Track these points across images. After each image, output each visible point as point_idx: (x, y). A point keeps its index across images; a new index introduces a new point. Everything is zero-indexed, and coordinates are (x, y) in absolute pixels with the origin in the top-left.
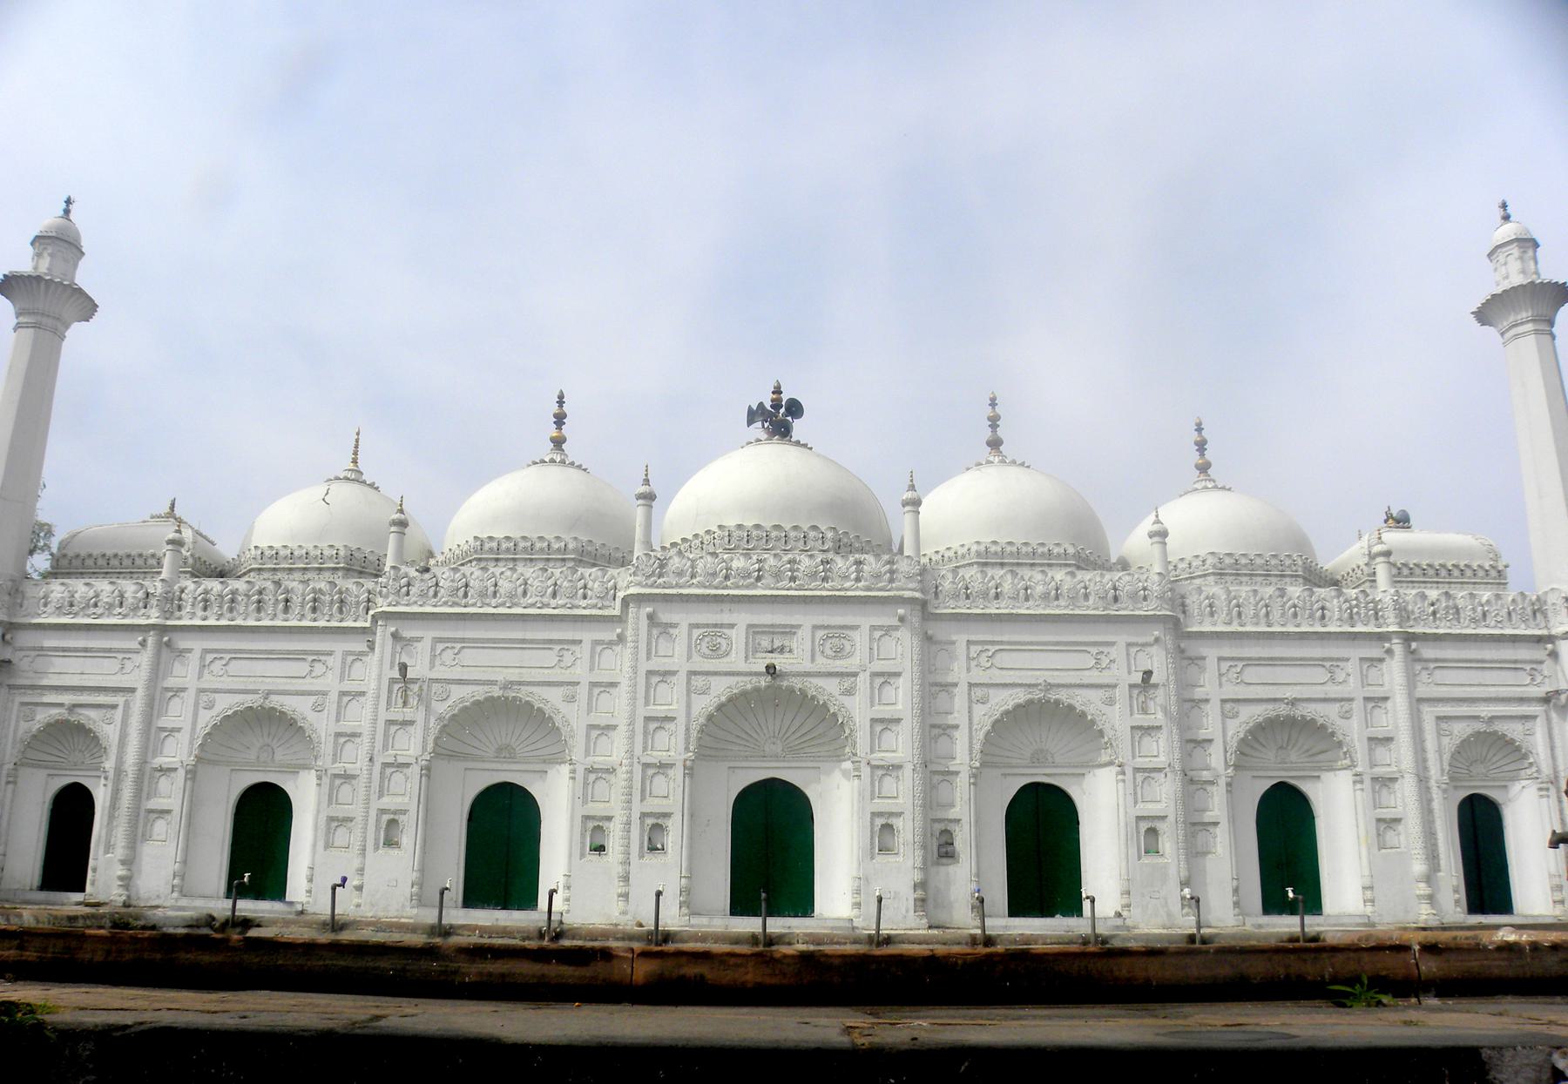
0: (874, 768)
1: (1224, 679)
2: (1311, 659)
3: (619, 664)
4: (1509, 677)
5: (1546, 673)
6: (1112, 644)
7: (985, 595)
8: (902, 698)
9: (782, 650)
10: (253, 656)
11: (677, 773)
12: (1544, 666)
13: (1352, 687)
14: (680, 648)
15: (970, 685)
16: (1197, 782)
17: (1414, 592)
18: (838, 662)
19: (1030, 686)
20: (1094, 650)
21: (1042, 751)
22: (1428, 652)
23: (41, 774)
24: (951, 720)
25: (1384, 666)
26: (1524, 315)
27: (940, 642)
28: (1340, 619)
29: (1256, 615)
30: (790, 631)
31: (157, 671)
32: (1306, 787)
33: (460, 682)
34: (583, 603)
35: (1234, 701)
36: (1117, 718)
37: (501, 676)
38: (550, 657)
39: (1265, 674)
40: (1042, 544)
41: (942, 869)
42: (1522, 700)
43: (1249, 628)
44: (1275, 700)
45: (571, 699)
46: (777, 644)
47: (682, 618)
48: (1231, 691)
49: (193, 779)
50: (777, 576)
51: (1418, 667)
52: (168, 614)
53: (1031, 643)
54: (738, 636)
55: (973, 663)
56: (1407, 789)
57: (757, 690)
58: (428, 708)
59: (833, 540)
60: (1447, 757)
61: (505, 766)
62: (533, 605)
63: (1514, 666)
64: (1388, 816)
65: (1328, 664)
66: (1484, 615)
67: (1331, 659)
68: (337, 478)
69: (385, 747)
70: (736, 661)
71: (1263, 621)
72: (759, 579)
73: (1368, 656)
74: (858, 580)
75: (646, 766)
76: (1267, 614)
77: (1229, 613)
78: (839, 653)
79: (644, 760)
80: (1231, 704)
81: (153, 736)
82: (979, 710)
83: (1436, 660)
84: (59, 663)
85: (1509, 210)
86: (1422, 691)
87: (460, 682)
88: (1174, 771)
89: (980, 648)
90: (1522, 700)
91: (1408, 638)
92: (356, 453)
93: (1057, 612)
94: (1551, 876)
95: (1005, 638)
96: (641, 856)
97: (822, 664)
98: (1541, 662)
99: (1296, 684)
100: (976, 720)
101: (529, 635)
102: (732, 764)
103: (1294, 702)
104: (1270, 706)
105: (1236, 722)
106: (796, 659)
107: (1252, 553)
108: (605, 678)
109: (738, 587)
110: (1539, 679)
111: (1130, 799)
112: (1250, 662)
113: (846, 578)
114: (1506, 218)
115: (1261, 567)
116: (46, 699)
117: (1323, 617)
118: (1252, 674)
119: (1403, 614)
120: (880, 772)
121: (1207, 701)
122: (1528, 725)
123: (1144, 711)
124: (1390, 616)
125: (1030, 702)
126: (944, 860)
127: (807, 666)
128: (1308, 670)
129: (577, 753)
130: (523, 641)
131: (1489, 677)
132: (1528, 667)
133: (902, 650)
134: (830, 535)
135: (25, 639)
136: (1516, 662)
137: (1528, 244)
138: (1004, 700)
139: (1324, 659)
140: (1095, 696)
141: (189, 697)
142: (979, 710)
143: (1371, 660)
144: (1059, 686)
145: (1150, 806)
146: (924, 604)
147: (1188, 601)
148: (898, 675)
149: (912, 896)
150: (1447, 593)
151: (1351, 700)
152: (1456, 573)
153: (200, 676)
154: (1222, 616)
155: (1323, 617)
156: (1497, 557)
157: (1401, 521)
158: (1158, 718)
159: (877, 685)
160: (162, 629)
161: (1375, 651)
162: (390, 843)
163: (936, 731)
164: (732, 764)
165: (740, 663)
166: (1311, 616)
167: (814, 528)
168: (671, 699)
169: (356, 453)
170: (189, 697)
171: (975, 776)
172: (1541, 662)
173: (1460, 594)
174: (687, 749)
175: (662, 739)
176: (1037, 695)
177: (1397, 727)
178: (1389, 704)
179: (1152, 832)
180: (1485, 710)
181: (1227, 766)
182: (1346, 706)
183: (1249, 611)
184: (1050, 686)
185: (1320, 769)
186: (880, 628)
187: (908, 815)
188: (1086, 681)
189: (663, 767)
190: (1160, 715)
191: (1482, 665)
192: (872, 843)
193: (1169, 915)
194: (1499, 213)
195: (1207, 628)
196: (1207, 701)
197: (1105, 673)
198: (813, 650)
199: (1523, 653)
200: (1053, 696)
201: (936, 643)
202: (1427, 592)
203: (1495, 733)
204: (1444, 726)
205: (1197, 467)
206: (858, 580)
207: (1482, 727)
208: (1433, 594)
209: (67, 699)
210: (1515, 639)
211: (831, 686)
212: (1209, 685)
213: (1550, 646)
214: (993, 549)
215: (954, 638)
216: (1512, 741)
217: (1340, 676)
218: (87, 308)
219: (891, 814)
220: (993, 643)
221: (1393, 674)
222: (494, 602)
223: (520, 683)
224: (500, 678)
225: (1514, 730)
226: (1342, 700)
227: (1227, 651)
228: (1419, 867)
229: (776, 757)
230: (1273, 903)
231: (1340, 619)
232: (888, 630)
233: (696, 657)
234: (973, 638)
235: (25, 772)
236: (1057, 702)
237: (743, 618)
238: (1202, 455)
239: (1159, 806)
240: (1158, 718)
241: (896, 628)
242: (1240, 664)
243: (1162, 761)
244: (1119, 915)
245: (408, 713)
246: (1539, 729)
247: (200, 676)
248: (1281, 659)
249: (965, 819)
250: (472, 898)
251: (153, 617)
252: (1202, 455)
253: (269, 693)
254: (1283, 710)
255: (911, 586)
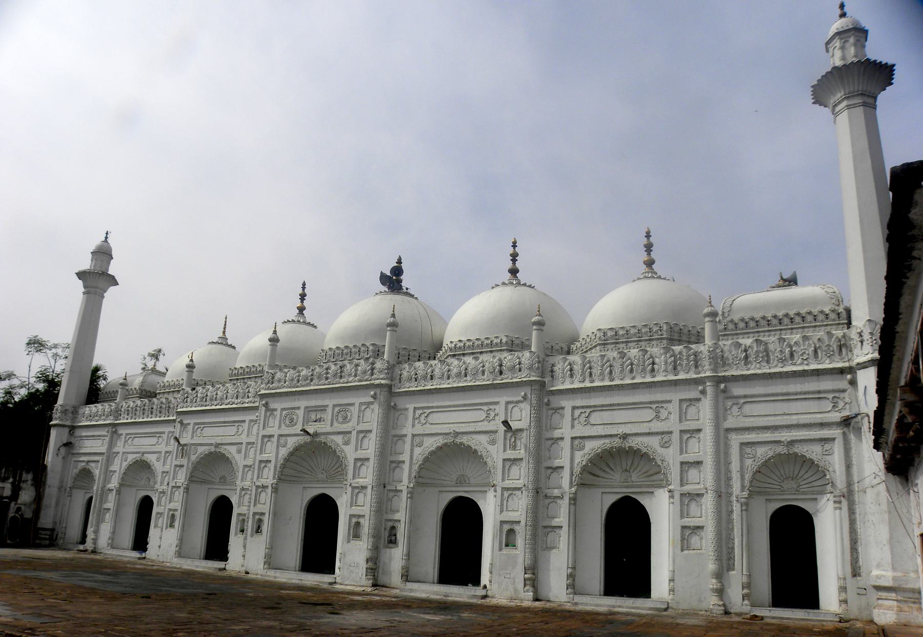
0: (354, 488)
1: (576, 422)
2: (641, 403)
4: (813, 406)
5: (847, 400)
6: (497, 403)
7: (425, 378)
9: (319, 420)
12: (846, 395)
13: (673, 424)
15: (414, 436)
16: (550, 497)
17: (730, 342)
18: (344, 426)
19: (446, 434)
20: (485, 408)
21: (463, 475)
22: (738, 390)
23: (82, 492)
24: (401, 458)
25: (700, 404)
26: (839, 95)
27: (400, 410)
28: (665, 371)
29: (602, 374)
31: (111, 445)
32: (645, 501)
33: (201, 445)
34: (247, 400)
35: (581, 438)
39: (606, 416)
40: (487, 338)
41: (388, 550)
42: (822, 425)
43: (597, 384)
44: (611, 436)
45: (493, 442)
46: (318, 417)
47: (276, 405)
48: (580, 431)
49: (575, 504)
50: (319, 377)
51: (729, 403)
53: (450, 406)
55: (417, 421)
57: (306, 443)
58: (189, 459)
59: (373, 352)
60: (748, 477)
61: (222, 487)
62: (228, 404)
63: (818, 396)
64: (692, 524)
65: (654, 406)
66: (792, 355)
67: (657, 402)
68: (639, 279)
69: (173, 479)
71: (607, 378)
72: (312, 380)
73: (836, 388)
74: (355, 376)
75: (258, 487)
76: (611, 372)
77: (583, 373)
78: (345, 420)
79: (258, 484)
80: (578, 441)
81: (108, 473)
82: (417, 451)
83: (745, 396)
84: (88, 443)
85: (846, 9)
86: (730, 423)
87: (201, 445)
88: (528, 490)
89: (421, 411)
90: (822, 425)
91: (718, 380)
92: (225, 328)
93: (465, 384)
94: (839, 578)
95: (435, 405)
96: (252, 536)
97: (338, 427)
98: (844, 391)
100: (415, 458)
101: (227, 419)
102: (441, 489)
103: (625, 437)
104: (607, 441)
105: (582, 453)
107: (627, 325)
108: (692, 425)
109: (303, 386)
110: (841, 404)
111: (498, 509)
112: (595, 408)
113: (350, 375)
114: (843, 15)
115: (635, 334)
116: (81, 459)
117: (653, 370)
120: (357, 491)
121: (562, 439)
122: (827, 446)
123: (514, 447)
124: (706, 363)
125: (446, 444)
126: (391, 545)
127: (328, 429)
128: (639, 412)
129: (498, 479)
130: (224, 422)
131: (795, 407)
132: (830, 396)
134: (371, 348)
135: (78, 432)
136: (819, 392)
137: (860, 33)
138: (431, 444)
139: (651, 403)
140: (483, 438)
142: (417, 451)
143: (690, 400)
144: (463, 433)
145: (510, 514)
146: (390, 387)
147: (555, 368)
148: (370, 431)
149: (365, 566)
150: (757, 340)
151: (671, 432)
152: (786, 321)
153: (573, 427)
154: (578, 377)
155: (653, 370)
156: (839, 302)
157: (792, 281)
158: (521, 453)
159: (360, 438)
160: (114, 425)
161: (693, 394)
162: (172, 526)
163: (394, 465)
164: (441, 489)
166: (644, 370)
167: (363, 345)
169: (225, 328)
171: (412, 494)
172: (844, 391)
173: (772, 340)
174: (274, 478)
175: (515, 471)
176: (450, 440)
177: (705, 453)
178: (701, 435)
179: (511, 532)
180: (786, 436)
181: (571, 486)
182: (666, 438)
183: (596, 371)
184: (457, 434)
185: (653, 486)
186: (364, 403)
187: (367, 517)
188: (478, 430)
189: (264, 487)
190: (523, 451)
191: (788, 398)
192: (349, 533)
193: (516, 590)
194: (839, 12)
195: (567, 386)
196: (562, 439)
197: (492, 423)
198: (332, 419)
199: (827, 384)
200: (458, 440)
201: (398, 410)
202: (740, 341)
203: (796, 454)
204: (748, 450)
205: (645, 263)
206: (355, 376)
207: (781, 449)
208: (747, 341)
210: (817, 373)
211: (339, 439)
212: (565, 430)
213: (849, 376)
214: (459, 344)
215: (407, 406)
216: (812, 462)
217: (664, 414)
218: (113, 281)
219: (359, 516)
220: (428, 408)
222: (215, 403)
223: (222, 444)
224: (213, 442)
225: (813, 452)
226: (663, 433)
227: (579, 402)
228: (711, 566)
229: (323, 482)
230: (612, 588)
231: (665, 371)
232: (369, 404)
233: (283, 427)
234: (417, 406)
235: (74, 491)
236: (461, 443)
237: (303, 403)
238: (649, 254)
239: (516, 514)
240: (521, 453)
241: (372, 403)
242: (588, 410)
243: (519, 483)
244: (243, 566)
246: (837, 449)
247: (573, 427)
248: (619, 405)
249: (403, 520)
250: (778, 600)
252: (649, 254)
253: (144, 453)
254: (617, 442)
255: (381, 376)
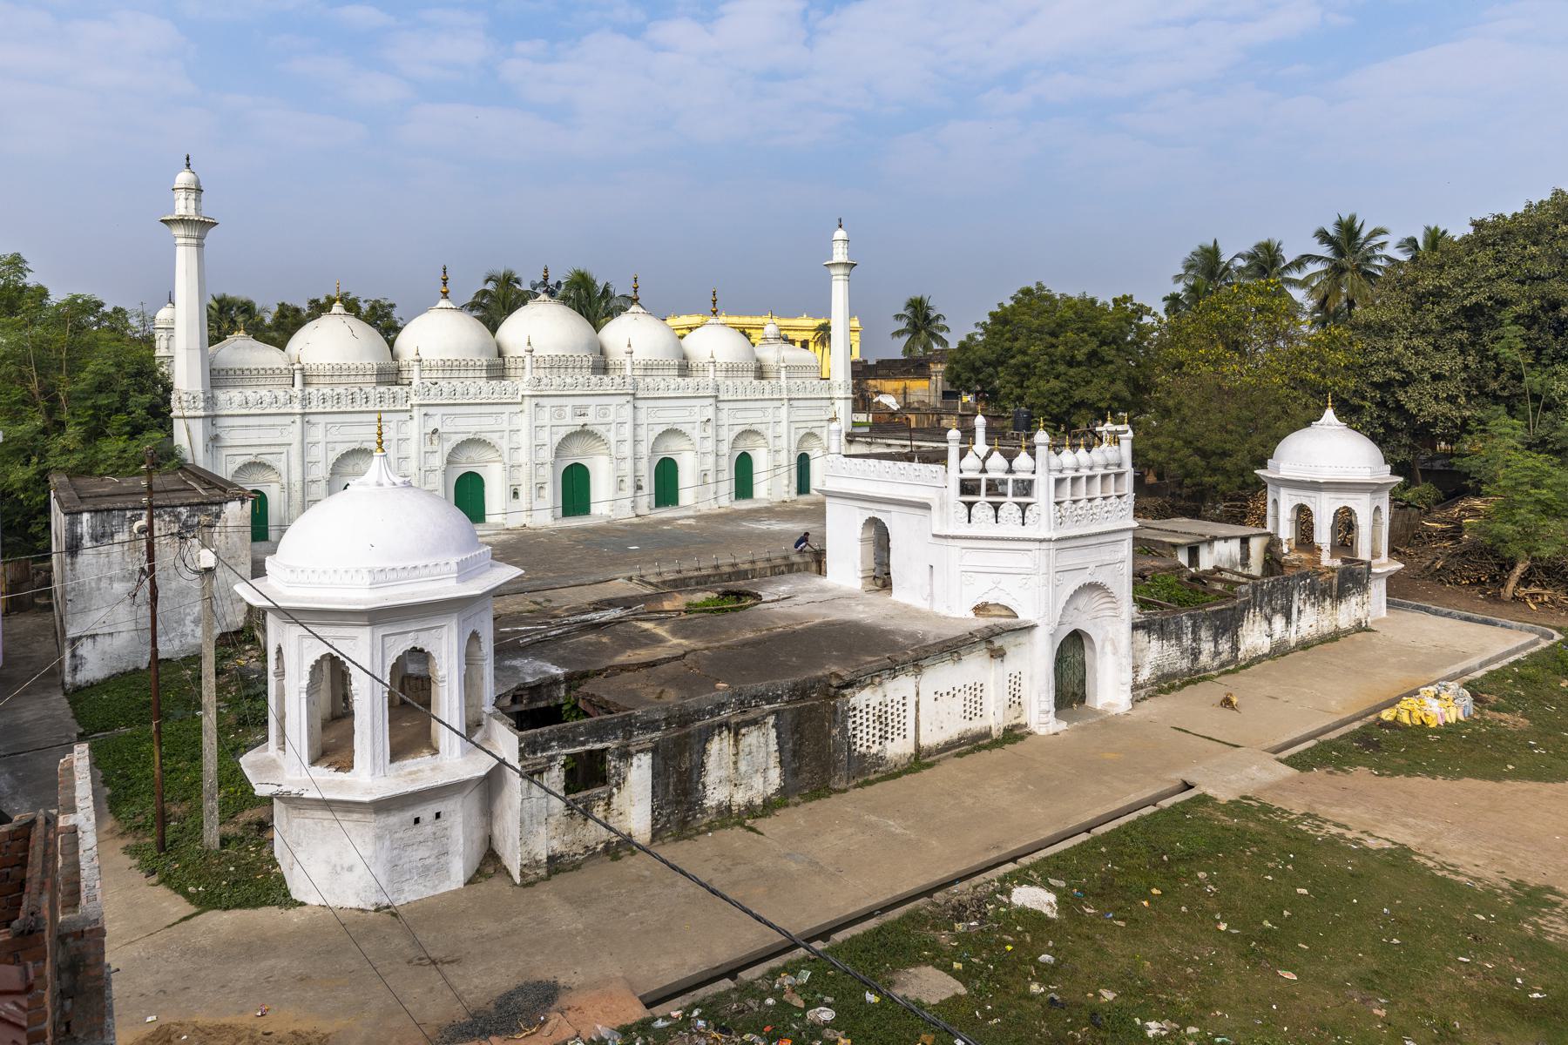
3: (523, 422)
8: (627, 431)
10: (352, 424)
11: (548, 467)
14: (547, 416)
22: (795, 403)
30: (587, 407)
36: (696, 434)
37: (473, 429)
38: (491, 420)
39: (743, 414)
52: (304, 407)
54: (568, 410)
56: (784, 454)
63: (820, 408)
70: (568, 420)
84: (235, 434)
99: (751, 418)
106: (590, 419)
118: (739, 414)
119: (789, 390)
133: (627, 411)
135: (222, 422)
141: (321, 446)
160: (303, 414)
165: (572, 422)
168: (545, 436)
170: (321, 446)
180: (810, 425)
209: (255, 451)
221: (784, 410)
245: (435, 448)
251: (297, 408)
